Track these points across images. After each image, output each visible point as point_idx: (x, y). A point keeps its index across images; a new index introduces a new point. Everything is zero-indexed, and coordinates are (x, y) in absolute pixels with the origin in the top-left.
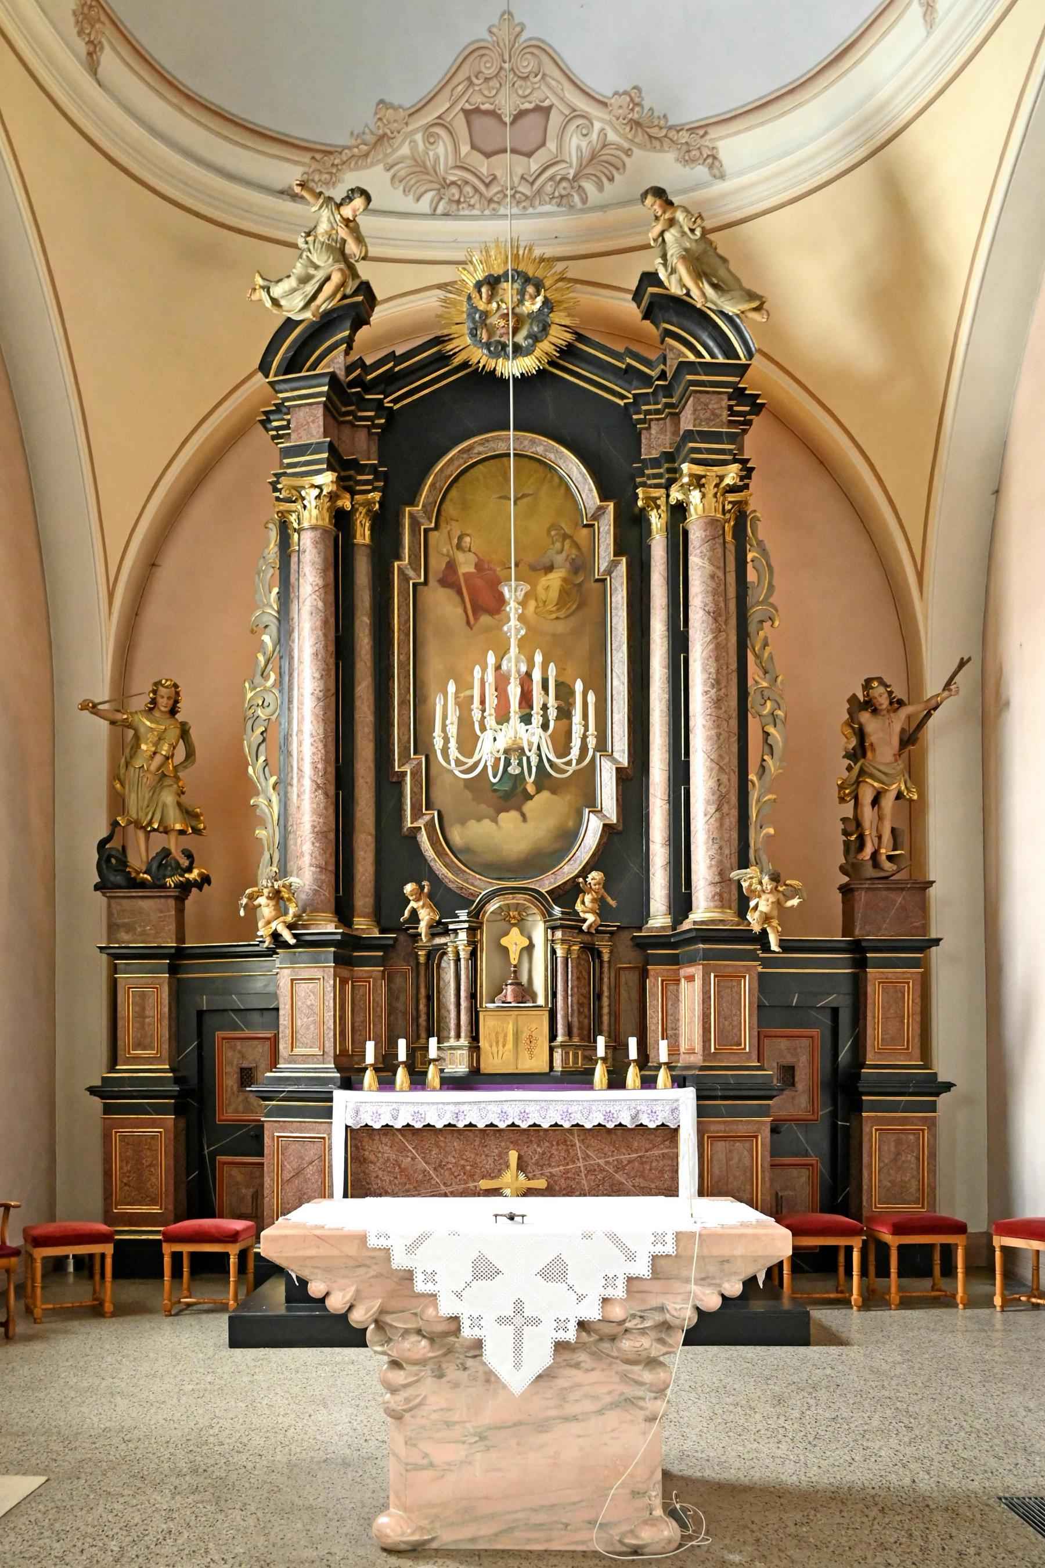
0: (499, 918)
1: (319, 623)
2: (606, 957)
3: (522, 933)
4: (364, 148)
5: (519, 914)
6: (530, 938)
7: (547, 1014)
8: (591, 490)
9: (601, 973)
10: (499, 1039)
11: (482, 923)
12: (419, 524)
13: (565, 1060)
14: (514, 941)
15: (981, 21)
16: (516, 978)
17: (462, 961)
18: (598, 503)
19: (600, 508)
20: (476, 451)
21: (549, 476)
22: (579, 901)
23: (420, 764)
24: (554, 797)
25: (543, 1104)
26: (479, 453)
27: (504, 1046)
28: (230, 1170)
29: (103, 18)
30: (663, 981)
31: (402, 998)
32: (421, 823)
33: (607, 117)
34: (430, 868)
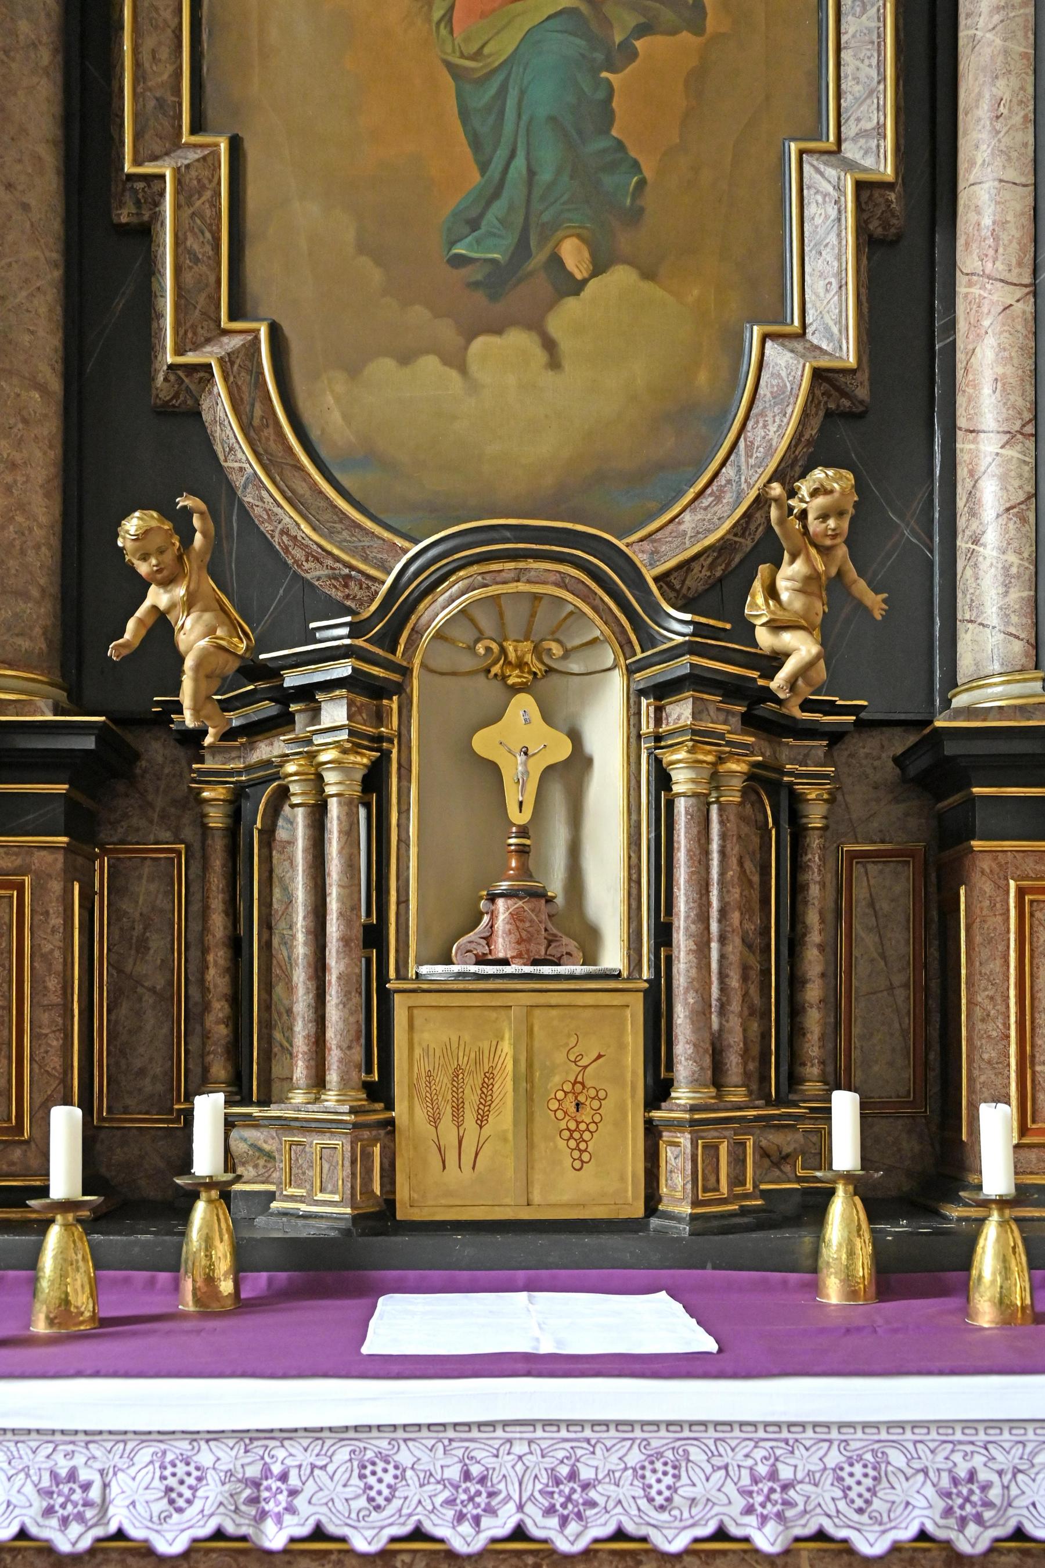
0: (467, 663)
2: (815, 816)
3: (548, 718)
5: (537, 650)
6: (575, 737)
7: (637, 1004)
9: (798, 866)
10: (466, 1091)
11: (406, 672)
13: (703, 1179)
16: (525, 872)
17: (334, 808)
22: (757, 585)
23: (211, 161)
24: (647, 286)
25: (659, 1440)
27: (481, 1121)
28: (276, 1087)
30: (1021, 892)
31: (156, 942)
32: (209, 355)
34: (244, 512)
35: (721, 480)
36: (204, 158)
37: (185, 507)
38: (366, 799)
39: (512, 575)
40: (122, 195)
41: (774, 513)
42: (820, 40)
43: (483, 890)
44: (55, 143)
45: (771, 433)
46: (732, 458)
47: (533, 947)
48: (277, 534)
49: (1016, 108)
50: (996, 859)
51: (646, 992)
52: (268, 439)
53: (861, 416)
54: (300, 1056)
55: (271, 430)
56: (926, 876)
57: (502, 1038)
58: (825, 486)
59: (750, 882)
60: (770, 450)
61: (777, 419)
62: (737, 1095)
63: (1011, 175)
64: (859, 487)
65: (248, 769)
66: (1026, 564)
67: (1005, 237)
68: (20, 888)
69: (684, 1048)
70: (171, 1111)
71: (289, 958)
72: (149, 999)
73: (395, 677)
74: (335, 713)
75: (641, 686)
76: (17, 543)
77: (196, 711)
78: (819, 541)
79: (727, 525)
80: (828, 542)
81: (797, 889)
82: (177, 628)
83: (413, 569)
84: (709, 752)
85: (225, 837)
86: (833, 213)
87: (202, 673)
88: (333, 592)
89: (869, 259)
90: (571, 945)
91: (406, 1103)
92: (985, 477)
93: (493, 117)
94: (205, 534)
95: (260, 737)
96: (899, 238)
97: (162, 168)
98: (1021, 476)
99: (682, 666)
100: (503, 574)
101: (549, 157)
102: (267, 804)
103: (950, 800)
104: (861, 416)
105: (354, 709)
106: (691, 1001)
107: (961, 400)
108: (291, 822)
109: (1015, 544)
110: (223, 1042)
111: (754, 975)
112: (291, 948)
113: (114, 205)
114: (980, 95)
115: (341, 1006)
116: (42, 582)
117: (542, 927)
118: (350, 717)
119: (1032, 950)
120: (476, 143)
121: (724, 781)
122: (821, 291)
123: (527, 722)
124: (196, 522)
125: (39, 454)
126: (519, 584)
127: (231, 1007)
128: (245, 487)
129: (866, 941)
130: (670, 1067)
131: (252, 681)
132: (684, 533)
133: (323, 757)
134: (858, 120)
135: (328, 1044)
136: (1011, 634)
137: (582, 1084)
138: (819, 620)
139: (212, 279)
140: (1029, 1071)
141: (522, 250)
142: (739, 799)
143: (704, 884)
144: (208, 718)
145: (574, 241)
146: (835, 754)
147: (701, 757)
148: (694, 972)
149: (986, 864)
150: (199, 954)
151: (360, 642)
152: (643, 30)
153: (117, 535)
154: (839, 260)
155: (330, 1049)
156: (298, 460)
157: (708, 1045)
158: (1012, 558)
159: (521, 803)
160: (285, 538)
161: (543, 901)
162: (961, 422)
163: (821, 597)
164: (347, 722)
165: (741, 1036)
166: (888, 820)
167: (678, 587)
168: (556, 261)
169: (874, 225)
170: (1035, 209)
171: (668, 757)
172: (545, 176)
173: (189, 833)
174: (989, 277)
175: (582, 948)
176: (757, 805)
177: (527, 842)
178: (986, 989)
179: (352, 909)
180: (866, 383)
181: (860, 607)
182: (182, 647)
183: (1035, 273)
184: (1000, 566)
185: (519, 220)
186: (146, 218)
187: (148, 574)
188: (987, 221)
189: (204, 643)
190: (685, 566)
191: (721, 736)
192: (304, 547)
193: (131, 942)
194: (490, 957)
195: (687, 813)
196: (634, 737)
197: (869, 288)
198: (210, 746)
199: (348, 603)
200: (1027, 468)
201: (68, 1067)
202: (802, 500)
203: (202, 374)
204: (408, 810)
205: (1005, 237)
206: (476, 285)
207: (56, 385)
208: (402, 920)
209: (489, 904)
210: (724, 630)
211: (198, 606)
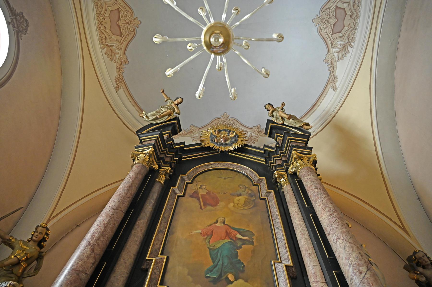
12: (185, 181)
15: (351, 79)
18: (259, 177)
19: (260, 179)
20: (210, 166)
23: (163, 259)
24: (246, 283)
29: (123, 83)
97: (153, 259)
101: (226, 262)
120: (212, 259)
139: (158, 278)
141: (220, 276)
152: (243, 244)
168: (227, 278)
169: (291, 274)
172: (226, 264)
183: (326, 280)
205: (317, 274)
206: (210, 281)
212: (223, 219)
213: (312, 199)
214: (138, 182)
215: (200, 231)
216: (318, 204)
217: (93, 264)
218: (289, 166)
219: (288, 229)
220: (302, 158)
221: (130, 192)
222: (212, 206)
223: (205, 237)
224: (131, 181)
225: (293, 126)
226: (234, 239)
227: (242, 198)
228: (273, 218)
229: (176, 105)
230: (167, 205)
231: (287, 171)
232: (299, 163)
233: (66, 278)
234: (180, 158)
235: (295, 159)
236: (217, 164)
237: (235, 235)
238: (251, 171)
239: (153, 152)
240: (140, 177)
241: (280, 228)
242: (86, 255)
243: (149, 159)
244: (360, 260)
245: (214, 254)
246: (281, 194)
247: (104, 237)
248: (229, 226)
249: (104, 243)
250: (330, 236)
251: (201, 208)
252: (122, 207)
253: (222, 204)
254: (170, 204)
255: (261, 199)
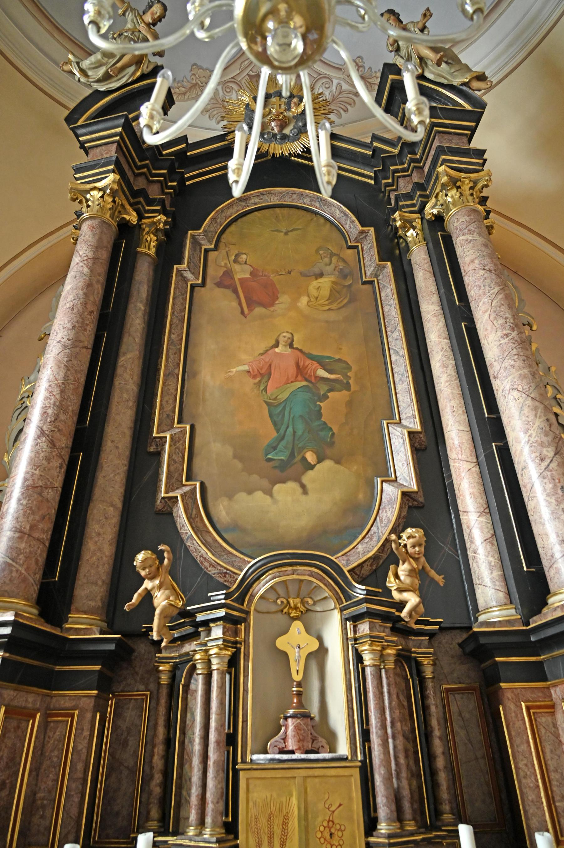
0: (273, 608)
1: (81, 284)
2: (428, 673)
3: (308, 631)
4: (183, 89)
5: (302, 602)
6: (320, 639)
7: (356, 773)
8: (353, 222)
9: (424, 697)
11: (248, 613)
14: (295, 641)
16: (300, 705)
17: (215, 676)
18: (360, 228)
19: (362, 232)
20: (252, 201)
21: (315, 219)
22: (390, 574)
23: (183, 432)
24: (337, 466)
26: (255, 204)
30: (528, 709)
31: (132, 742)
32: (177, 494)
33: (342, 76)
34: (187, 549)
35: (372, 532)
36: (181, 431)
37: (161, 549)
38: (230, 670)
39: (291, 572)
40: (152, 443)
41: (394, 546)
42: (390, 395)
43: (281, 714)
44: (131, 428)
45: (389, 515)
46: (375, 524)
47: (305, 744)
48: (198, 557)
49: (459, 409)
50: (513, 692)
51: (361, 768)
52: (197, 522)
53: (422, 507)
54: (194, 807)
55: (199, 518)
56: (483, 700)
57: (292, 795)
58: (411, 536)
59: (403, 705)
60: (389, 521)
61: (390, 509)
62: (410, 826)
63: (462, 428)
64: (426, 534)
65: (180, 656)
66: (497, 561)
67: (464, 447)
68: (72, 716)
69: (381, 799)
70: (129, 837)
71: (192, 750)
72: (125, 772)
73: (243, 615)
74: (217, 632)
75: (346, 617)
76: (96, 563)
77: (159, 632)
78: (413, 556)
79: (376, 549)
80: (417, 556)
81: (425, 708)
82: (154, 597)
83: (251, 571)
84: (378, 646)
85: (167, 688)
86: (401, 441)
87: (162, 616)
88: (220, 579)
89: (417, 456)
90: (323, 742)
91: (245, 835)
92: (474, 528)
93: (281, 416)
94: (169, 559)
95: (186, 641)
96: (426, 449)
97: (165, 435)
98: (487, 528)
99: (363, 608)
100: (287, 572)
101: (300, 427)
102: (187, 673)
103: (487, 663)
104: (422, 507)
105: (225, 630)
106: (383, 772)
107: (459, 501)
108: (197, 680)
109: (491, 554)
110: (158, 797)
111: (411, 754)
112: (193, 745)
113: (148, 445)
114: (446, 405)
115: (214, 779)
116: (103, 578)
117: (309, 733)
118: (224, 634)
119: (540, 739)
120: (275, 424)
121: (386, 658)
122: (401, 466)
123: (299, 633)
124: (166, 555)
125: (109, 530)
126: (294, 576)
127: (163, 776)
128: (187, 539)
129: (461, 734)
130: (375, 810)
131: (184, 618)
132: (359, 553)
133: (211, 652)
134: (406, 414)
135: (207, 801)
136: (497, 590)
137: (333, 822)
138: (417, 586)
139: (181, 468)
140: (553, 806)
141: (292, 455)
142: (393, 667)
143: (382, 709)
144: (164, 634)
145: (311, 452)
146: (433, 643)
147: (375, 648)
148: (382, 756)
149: (509, 695)
150: (151, 747)
151: (228, 601)
152: (330, 390)
153: (134, 560)
154: (406, 456)
155: (208, 804)
156: (208, 529)
157: (392, 797)
158: (491, 559)
159: (298, 671)
160: (201, 558)
161: (309, 719)
162: (460, 508)
163: (417, 578)
164: (222, 636)
165: (408, 791)
166: (460, 673)
167: (358, 573)
168: (304, 459)
170: (469, 423)
171: (361, 648)
172: (299, 433)
173: (152, 686)
174: (461, 460)
175: (329, 743)
176: (402, 667)
177: (301, 689)
178: (522, 760)
179: (222, 726)
180: (422, 496)
181: (432, 580)
182: (155, 605)
183: (477, 458)
184: (487, 562)
185: (290, 446)
186: (159, 450)
187: (145, 576)
188: (456, 442)
189: (165, 603)
190: (361, 565)
191: (383, 638)
192: (208, 561)
193: (119, 742)
194: (285, 749)
195: (371, 674)
196: (346, 639)
197: (418, 464)
198: (164, 647)
199: (226, 583)
200: (489, 525)
201: (81, 813)
202: (404, 540)
203: (174, 500)
204: (248, 675)
205: (464, 447)
206: (275, 467)
207: (120, 505)
208: (244, 730)
209: (285, 721)
210: (379, 592)
211: (164, 588)
212: (290, 336)
213: (472, 292)
214: (102, 270)
215: (246, 368)
216: (483, 309)
217: (61, 467)
218: (428, 197)
219: (416, 351)
220: (458, 184)
221: (92, 298)
222: (265, 306)
223: (258, 379)
224: (86, 270)
225: (445, 82)
226: (313, 380)
227: (326, 283)
228: (389, 329)
229: (148, 25)
230: (173, 313)
231: (421, 210)
232: (452, 197)
233: (21, 504)
234: (182, 180)
235: (444, 186)
236: (268, 194)
237: (315, 372)
238: (342, 211)
239: (119, 183)
240: (105, 255)
241: (401, 353)
242: (42, 454)
243: (114, 201)
244: (546, 435)
245: (276, 412)
246: (406, 268)
247: (65, 412)
248: (301, 351)
249: (69, 422)
250: (498, 381)
251: (242, 313)
252: (82, 338)
253: (284, 299)
254: (177, 308)
255: (364, 283)
